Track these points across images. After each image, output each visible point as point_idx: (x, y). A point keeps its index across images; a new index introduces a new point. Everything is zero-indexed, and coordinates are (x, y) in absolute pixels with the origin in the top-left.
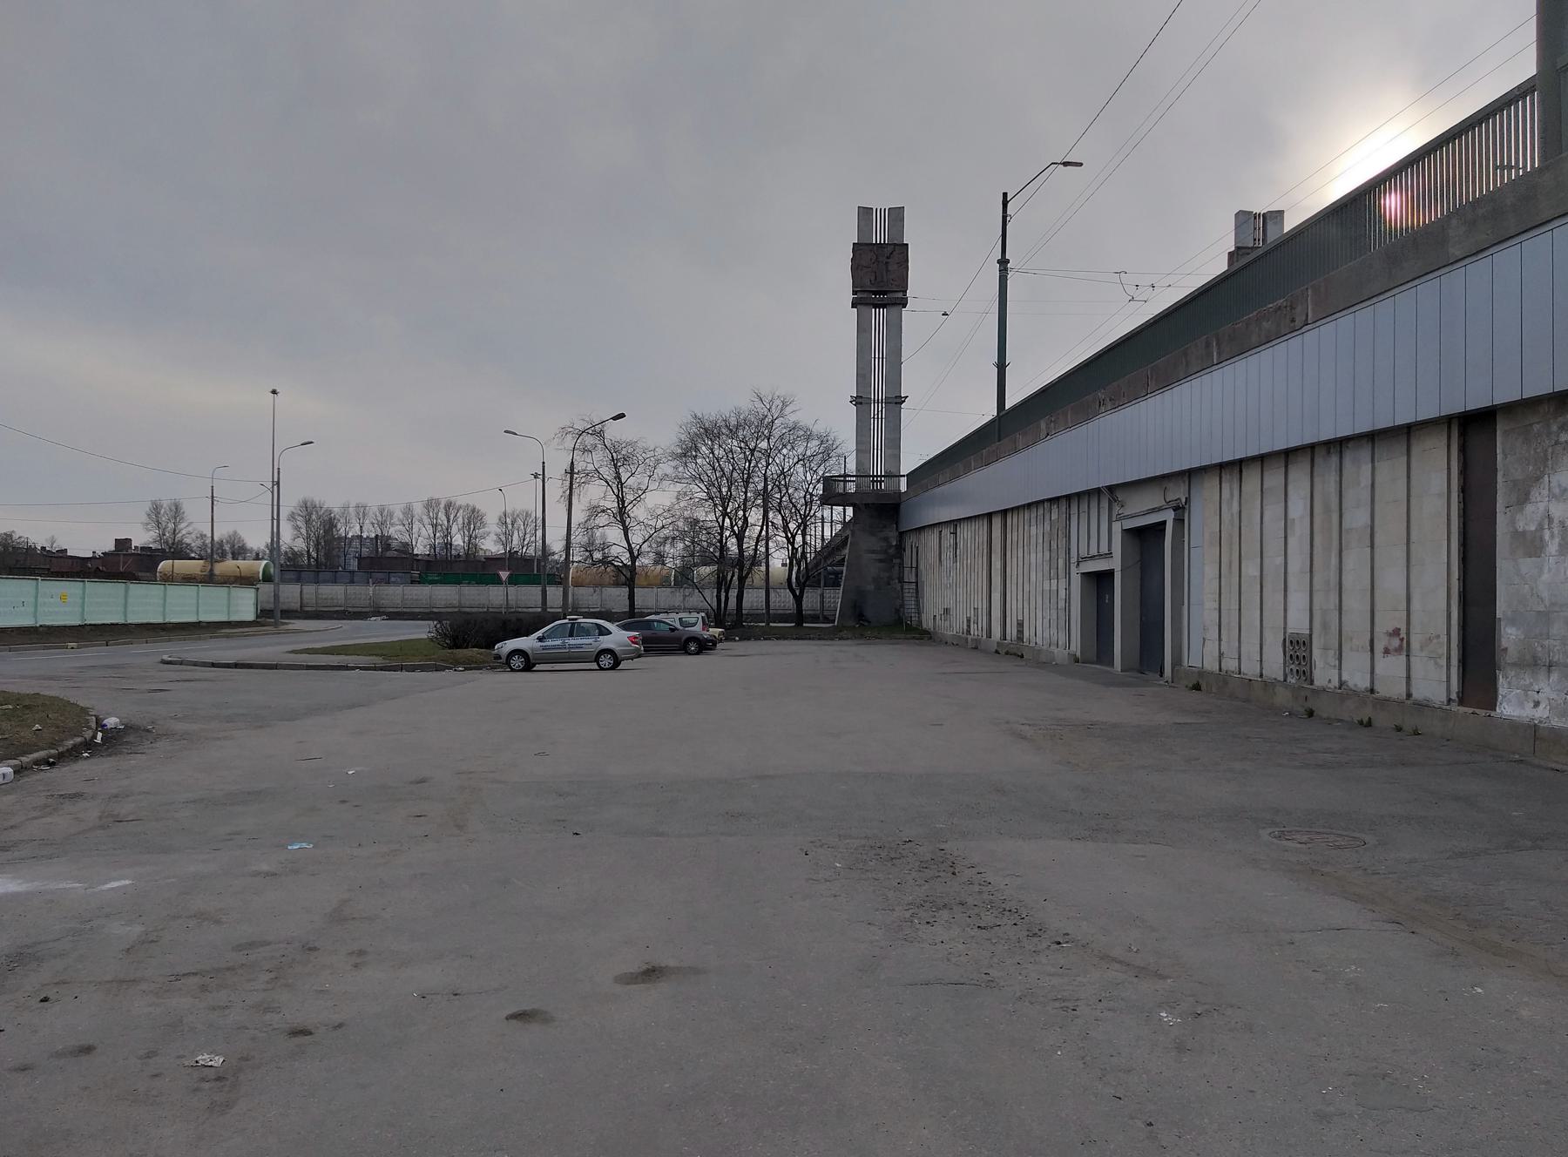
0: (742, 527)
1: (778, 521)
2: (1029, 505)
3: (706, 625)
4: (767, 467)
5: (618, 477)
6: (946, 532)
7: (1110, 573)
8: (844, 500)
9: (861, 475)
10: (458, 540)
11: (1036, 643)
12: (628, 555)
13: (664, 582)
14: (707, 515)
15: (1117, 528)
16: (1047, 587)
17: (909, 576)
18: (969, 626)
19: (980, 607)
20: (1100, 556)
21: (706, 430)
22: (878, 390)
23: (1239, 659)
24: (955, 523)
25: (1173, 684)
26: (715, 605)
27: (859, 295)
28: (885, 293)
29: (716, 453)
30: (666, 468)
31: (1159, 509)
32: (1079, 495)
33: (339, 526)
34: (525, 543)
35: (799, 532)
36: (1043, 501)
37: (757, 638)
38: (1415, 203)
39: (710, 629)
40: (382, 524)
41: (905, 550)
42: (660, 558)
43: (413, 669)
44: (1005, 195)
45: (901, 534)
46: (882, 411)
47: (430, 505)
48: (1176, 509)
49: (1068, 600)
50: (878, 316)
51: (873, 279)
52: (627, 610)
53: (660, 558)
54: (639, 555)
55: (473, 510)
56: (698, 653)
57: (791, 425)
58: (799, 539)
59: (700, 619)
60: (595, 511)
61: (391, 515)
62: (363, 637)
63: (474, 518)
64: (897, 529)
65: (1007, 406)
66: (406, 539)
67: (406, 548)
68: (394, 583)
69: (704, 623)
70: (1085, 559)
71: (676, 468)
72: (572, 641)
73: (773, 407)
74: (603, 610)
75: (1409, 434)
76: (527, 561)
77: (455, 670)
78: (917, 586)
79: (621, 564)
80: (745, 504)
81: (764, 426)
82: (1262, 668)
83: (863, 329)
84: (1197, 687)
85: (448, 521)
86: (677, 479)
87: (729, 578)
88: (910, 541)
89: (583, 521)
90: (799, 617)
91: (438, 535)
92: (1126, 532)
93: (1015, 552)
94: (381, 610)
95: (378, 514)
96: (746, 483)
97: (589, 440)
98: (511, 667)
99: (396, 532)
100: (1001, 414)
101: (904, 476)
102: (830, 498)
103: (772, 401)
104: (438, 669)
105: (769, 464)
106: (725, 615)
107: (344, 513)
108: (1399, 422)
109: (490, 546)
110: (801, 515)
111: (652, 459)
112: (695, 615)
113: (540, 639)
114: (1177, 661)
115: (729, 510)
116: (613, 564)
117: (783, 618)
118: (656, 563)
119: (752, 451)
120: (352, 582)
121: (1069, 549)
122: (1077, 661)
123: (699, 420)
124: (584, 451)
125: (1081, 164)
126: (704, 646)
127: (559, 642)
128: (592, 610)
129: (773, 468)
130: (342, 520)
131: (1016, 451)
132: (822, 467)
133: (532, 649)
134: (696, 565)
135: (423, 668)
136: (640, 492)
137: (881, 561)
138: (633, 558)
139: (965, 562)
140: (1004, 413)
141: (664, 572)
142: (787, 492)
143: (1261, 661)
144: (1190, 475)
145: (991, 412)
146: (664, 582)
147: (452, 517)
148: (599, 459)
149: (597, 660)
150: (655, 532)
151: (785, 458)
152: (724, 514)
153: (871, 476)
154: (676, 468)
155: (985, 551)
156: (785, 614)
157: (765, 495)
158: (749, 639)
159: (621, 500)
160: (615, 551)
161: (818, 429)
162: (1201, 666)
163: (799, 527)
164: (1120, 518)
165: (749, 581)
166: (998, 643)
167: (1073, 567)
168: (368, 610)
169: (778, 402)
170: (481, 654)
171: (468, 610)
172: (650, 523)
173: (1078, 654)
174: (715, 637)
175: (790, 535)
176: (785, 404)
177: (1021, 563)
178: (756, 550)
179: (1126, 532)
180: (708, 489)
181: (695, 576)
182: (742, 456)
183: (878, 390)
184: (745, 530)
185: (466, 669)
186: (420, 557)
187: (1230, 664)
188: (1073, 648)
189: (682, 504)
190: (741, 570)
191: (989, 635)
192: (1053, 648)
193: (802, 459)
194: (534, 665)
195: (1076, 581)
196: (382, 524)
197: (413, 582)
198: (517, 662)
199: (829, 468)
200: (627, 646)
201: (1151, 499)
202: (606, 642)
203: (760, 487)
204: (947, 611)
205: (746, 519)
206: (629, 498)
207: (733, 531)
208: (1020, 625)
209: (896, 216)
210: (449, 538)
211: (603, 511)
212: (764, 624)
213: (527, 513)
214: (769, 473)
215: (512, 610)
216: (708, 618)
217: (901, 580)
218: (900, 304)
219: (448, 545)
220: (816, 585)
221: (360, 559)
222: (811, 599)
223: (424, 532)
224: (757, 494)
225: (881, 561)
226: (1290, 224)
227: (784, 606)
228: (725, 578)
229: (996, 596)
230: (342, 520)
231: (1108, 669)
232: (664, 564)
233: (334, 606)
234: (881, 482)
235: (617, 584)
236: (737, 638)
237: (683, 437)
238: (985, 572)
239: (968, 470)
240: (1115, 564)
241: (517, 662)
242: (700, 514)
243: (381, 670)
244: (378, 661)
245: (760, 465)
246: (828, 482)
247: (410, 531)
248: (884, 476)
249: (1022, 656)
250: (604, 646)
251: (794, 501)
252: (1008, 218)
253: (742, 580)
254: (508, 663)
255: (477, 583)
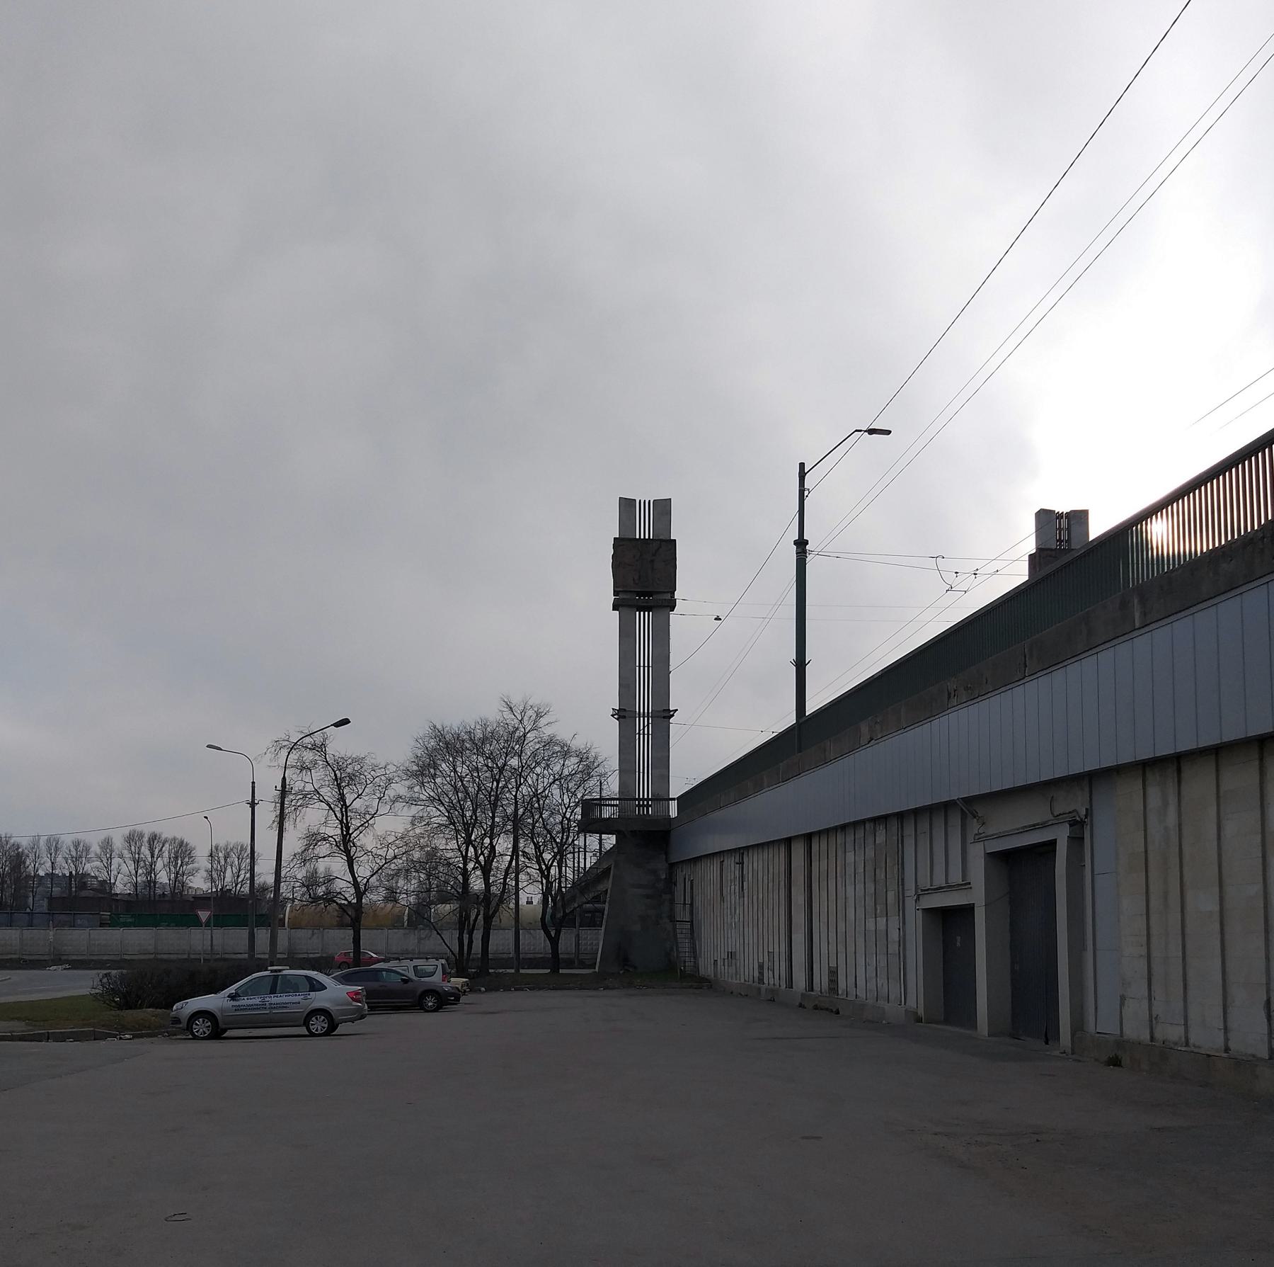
0: (489, 857)
1: (531, 850)
2: (844, 827)
3: (446, 975)
4: (518, 790)
5: (342, 798)
6: (730, 863)
7: (968, 910)
8: (602, 827)
9: (626, 796)
10: (163, 877)
11: (780, 986)
12: (352, 891)
13: (396, 923)
14: (448, 845)
15: (977, 854)
16: (871, 925)
17: (682, 914)
18: (761, 973)
19: (776, 950)
20: (950, 888)
21: (447, 743)
22: (643, 702)
23: (1186, 1025)
24: (741, 851)
25: (1074, 1056)
26: (456, 949)
27: (621, 596)
28: (650, 594)
29: (459, 769)
30: (399, 788)
31: (1044, 826)
32: (916, 812)
33: (28, 863)
34: (240, 880)
35: (555, 864)
36: (863, 822)
37: (507, 989)
38: (1186, 528)
39: (452, 979)
40: (76, 860)
41: (675, 885)
42: (392, 895)
43: (62, 1038)
44: (802, 465)
45: (672, 865)
46: (648, 725)
47: (133, 839)
48: (1073, 824)
49: (902, 942)
50: (643, 620)
51: (636, 578)
52: (615, 836)
53: (392, 895)
54: (366, 890)
55: (181, 844)
56: (435, 1010)
57: (546, 738)
58: (554, 871)
59: (440, 967)
60: (314, 839)
61: (87, 849)
62: (1000, 836)
63: (182, 852)
64: (666, 860)
65: (811, 708)
66: (103, 876)
67: (105, 886)
68: (80, 926)
69: (444, 972)
70: (927, 891)
71: (410, 788)
72: (274, 999)
73: (526, 718)
74: (324, 955)
75: (1217, 754)
76: (239, 900)
77: (121, 1038)
78: (692, 925)
79: (346, 902)
80: (492, 830)
81: (514, 740)
82: (1227, 1040)
83: (626, 634)
84: (1115, 1062)
85: (152, 856)
86: (412, 801)
87: (473, 917)
88: (680, 875)
89: (300, 851)
90: (555, 962)
91: (140, 871)
92: (992, 856)
93: (824, 884)
94: (64, 958)
95: (72, 849)
96: (494, 807)
97: (309, 756)
98: (193, 1034)
99: (91, 867)
100: (801, 721)
101: (674, 799)
102: (591, 824)
103: (524, 712)
104: (97, 1037)
105: (521, 784)
106: (468, 959)
107: (33, 848)
108: (1252, 733)
109: (199, 883)
110: (557, 843)
111: (383, 778)
112: (432, 961)
113: (233, 997)
114: (1078, 1025)
115: (473, 838)
116: (335, 902)
117: (533, 963)
118: (386, 899)
119: (501, 770)
120: (30, 925)
121: (903, 879)
122: (919, 1020)
123: (439, 734)
124: (302, 768)
125: (888, 432)
126: (444, 1000)
127: (256, 1000)
128: (311, 956)
129: (524, 789)
130: (32, 856)
131: (826, 762)
132: (581, 788)
133: (222, 1010)
134: (432, 903)
135: (77, 1037)
136: (368, 817)
137: (648, 897)
138: (359, 894)
139: (755, 897)
140: (804, 719)
141: (397, 910)
142: (541, 816)
143: (1226, 1029)
144: (1091, 779)
145: (791, 720)
146: (396, 923)
147: (157, 851)
148: (320, 777)
149: (306, 1023)
150: (386, 863)
151: (539, 778)
152: (468, 842)
153: (637, 799)
154: (410, 788)
155: (782, 883)
156: (535, 959)
157: (516, 821)
158: (497, 989)
159: (345, 826)
160: (339, 885)
161: (578, 744)
162: (1119, 1033)
163: (554, 857)
164: (979, 838)
165: (495, 921)
166: (802, 994)
167: (910, 903)
168: (46, 958)
169: (530, 712)
170: (156, 1016)
171: (165, 957)
172: (379, 852)
173: (921, 1012)
174: (457, 988)
175: (544, 867)
176: (539, 715)
177: (832, 897)
178: (505, 883)
179: (992, 856)
180: (449, 812)
181: (432, 914)
182: (488, 774)
183: (643, 702)
184: (492, 861)
185: (135, 1037)
186: (119, 897)
187: (1171, 1032)
188: (912, 1003)
189: (418, 831)
190: (487, 907)
191: (790, 984)
192: (881, 1003)
193: (559, 778)
194: (225, 1031)
195: (915, 922)
196: (76, 860)
197: (102, 925)
198: (201, 1027)
199: (589, 790)
200: (348, 1005)
201: (1034, 812)
202: (319, 1000)
203: (510, 810)
204: (731, 955)
205: (493, 848)
206: (355, 823)
207: (478, 862)
208: (833, 973)
209: (663, 508)
210: (153, 875)
211: (324, 839)
212: (513, 971)
213: (242, 846)
214: (519, 796)
215: (218, 956)
216: (449, 964)
217: (672, 919)
218: (668, 606)
219: (151, 883)
220: (572, 924)
221: (51, 899)
222: (567, 941)
223: (124, 868)
224: (506, 818)
225: (648, 897)
226: (1096, 529)
227: (534, 949)
228: (468, 917)
229: (799, 938)
230: (32, 856)
231: (968, 1032)
232: (396, 901)
233: (8, 954)
234: (648, 806)
235: (341, 925)
236: (483, 989)
237: (419, 753)
238: (782, 908)
239: (759, 787)
240: (977, 896)
241: (201, 1027)
242: (440, 842)
243: (20, 1040)
244: (19, 1027)
245: (510, 786)
246: (589, 806)
247: (108, 868)
248: (651, 800)
249: (838, 1012)
250: (317, 1005)
251: (548, 827)
252: (806, 493)
253: (488, 919)
254: (189, 1028)
255: (176, 926)
